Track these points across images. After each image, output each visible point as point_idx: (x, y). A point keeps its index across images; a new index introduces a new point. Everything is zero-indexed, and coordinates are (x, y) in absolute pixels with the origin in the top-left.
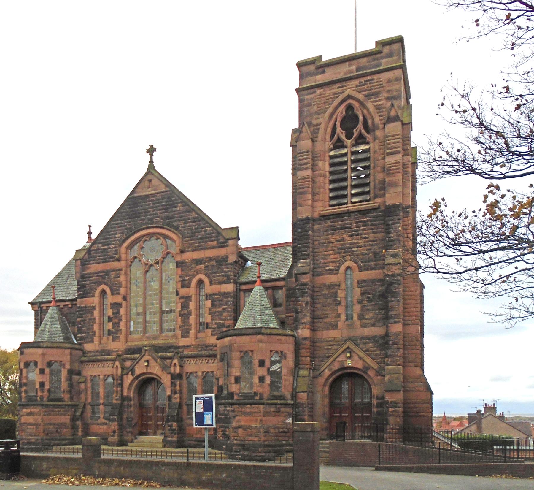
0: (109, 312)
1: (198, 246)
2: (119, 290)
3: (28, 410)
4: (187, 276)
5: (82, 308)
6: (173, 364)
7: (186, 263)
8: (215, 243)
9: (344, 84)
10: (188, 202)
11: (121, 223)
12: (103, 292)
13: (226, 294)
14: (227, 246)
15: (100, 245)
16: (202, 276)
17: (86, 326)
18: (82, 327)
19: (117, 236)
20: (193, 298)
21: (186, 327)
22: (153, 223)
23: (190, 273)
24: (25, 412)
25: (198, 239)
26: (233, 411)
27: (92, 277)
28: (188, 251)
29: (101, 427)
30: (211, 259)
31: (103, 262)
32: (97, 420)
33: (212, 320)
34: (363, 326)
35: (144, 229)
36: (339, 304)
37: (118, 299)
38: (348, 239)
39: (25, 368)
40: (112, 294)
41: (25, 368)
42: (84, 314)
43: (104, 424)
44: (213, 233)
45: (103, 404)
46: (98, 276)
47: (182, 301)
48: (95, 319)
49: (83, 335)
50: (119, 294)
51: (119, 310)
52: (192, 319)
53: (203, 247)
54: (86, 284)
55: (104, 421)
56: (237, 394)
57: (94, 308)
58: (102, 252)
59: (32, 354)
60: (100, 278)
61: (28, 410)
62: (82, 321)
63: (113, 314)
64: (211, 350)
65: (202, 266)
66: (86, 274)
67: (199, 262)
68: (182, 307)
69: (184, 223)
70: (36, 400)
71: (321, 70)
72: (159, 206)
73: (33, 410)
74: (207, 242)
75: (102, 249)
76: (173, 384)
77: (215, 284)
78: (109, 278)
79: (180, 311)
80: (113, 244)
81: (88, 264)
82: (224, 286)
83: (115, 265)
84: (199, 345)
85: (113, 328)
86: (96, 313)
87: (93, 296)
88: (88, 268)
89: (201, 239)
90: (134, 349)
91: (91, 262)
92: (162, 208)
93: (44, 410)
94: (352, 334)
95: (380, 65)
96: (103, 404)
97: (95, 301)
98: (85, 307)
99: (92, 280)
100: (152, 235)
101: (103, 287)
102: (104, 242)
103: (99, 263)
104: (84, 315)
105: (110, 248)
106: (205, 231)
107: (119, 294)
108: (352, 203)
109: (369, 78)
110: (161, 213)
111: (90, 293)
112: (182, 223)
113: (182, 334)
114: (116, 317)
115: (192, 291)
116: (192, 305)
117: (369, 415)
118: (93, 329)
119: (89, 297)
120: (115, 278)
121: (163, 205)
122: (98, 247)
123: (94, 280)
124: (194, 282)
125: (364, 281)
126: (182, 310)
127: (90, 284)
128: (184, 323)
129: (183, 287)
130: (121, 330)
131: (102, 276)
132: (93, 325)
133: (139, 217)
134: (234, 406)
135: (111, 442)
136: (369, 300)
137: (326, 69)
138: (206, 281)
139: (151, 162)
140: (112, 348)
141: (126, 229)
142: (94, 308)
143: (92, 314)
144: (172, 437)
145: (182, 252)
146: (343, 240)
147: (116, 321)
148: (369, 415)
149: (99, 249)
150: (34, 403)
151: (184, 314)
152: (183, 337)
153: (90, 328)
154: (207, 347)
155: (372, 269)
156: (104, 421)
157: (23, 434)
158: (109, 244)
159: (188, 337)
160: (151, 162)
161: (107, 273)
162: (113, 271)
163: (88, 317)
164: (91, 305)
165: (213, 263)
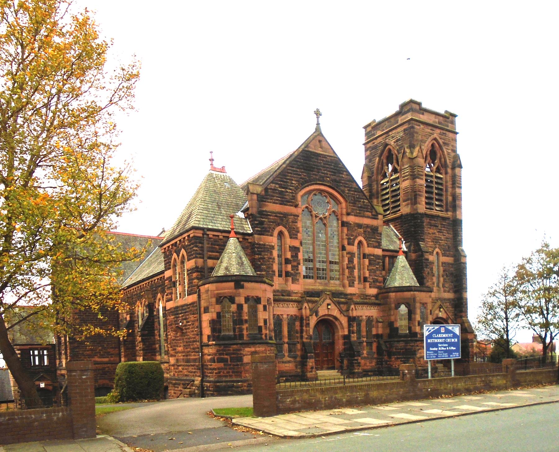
0: (289, 255)
1: (359, 213)
2: (297, 235)
3: (253, 349)
4: (352, 235)
5: (260, 244)
6: (304, 307)
7: (351, 224)
8: (369, 214)
9: (434, 129)
10: (290, 159)
11: (297, 171)
12: (281, 234)
13: (377, 257)
14: (377, 219)
15: (277, 186)
16: (360, 238)
17: (265, 265)
18: (262, 264)
19: (293, 182)
20: (356, 255)
21: (352, 278)
22: (324, 181)
23: (355, 234)
24: (248, 352)
25: (358, 207)
26: (417, 346)
27: (270, 216)
28: (352, 215)
29: (286, 365)
30: (367, 226)
31: (281, 204)
32: (282, 358)
33: (370, 275)
34: (445, 291)
35: (316, 184)
36: (434, 276)
37: (296, 243)
38: (437, 233)
39: (246, 303)
40: (368, 247)
41: (246, 303)
42: (264, 251)
43: (289, 362)
44: (369, 206)
45: (287, 343)
46: (276, 216)
47: (348, 255)
48: (274, 259)
49: (263, 273)
50: (297, 238)
51: (297, 254)
52: (356, 272)
53: (362, 215)
54: (264, 221)
55: (289, 359)
56: (419, 334)
57: (273, 247)
58: (280, 194)
59: (253, 289)
60: (278, 218)
61: (253, 349)
62: (261, 258)
63: (292, 256)
64: (369, 299)
65: (362, 230)
66: (264, 211)
67: (359, 226)
68: (349, 261)
69: (348, 190)
70: (262, 338)
71: (422, 111)
72: (327, 168)
73: (258, 349)
74: (364, 211)
75: (279, 190)
76: (350, 325)
77: (371, 247)
78: (287, 221)
79: (347, 264)
80: (291, 189)
81: (265, 202)
82: (376, 250)
83: (292, 210)
84: (362, 294)
85: (292, 270)
86: (275, 253)
87: (272, 236)
88: (266, 205)
89: (361, 207)
90: (312, 292)
91: (269, 200)
92: (332, 170)
93: (269, 348)
94: (440, 296)
95: (448, 126)
96: (287, 343)
97: (273, 240)
98: (264, 245)
99: (270, 219)
100: (321, 192)
101: (281, 228)
102: (281, 184)
103: (277, 204)
104: (263, 253)
105: (287, 192)
106: (364, 202)
107: (297, 238)
108: (436, 210)
109: (444, 132)
110: (330, 175)
111: (269, 231)
112: (346, 189)
113: (349, 283)
114: (294, 261)
115: (354, 249)
116: (356, 260)
117: (64, 366)
118: (272, 268)
119: (267, 235)
120: (292, 222)
121: (331, 168)
122: (275, 187)
123: (273, 219)
124: (276, 233)
125: (445, 263)
126: (349, 263)
127: (270, 222)
128: (351, 274)
129: (349, 244)
130: (299, 273)
131: (280, 217)
132: (272, 265)
133: (313, 171)
134: (418, 343)
135: (311, 378)
136: (447, 276)
137: (425, 113)
138: (365, 242)
139: (318, 124)
140: (292, 289)
141: (301, 178)
142: (273, 247)
143: (271, 253)
144: (358, 369)
145: (348, 214)
146: (434, 233)
147: (295, 264)
148: (64, 366)
149: (276, 190)
150: (259, 341)
151: (350, 267)
152: (350, 286)
153: (270, 267)
154: (367, 296)
155: (448, 256)
156: (289, 359)
157: (247, 375)
158: (287, 188)
159: (354, 286)
160: (318, 124)
161: (285, 215)
162: (291, 215)
163: (267, 255)
164: (271, 244)
165: (369, 230)
